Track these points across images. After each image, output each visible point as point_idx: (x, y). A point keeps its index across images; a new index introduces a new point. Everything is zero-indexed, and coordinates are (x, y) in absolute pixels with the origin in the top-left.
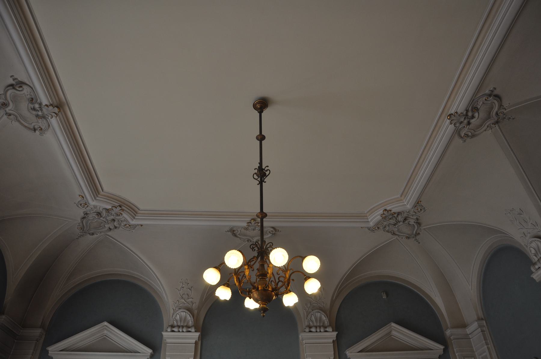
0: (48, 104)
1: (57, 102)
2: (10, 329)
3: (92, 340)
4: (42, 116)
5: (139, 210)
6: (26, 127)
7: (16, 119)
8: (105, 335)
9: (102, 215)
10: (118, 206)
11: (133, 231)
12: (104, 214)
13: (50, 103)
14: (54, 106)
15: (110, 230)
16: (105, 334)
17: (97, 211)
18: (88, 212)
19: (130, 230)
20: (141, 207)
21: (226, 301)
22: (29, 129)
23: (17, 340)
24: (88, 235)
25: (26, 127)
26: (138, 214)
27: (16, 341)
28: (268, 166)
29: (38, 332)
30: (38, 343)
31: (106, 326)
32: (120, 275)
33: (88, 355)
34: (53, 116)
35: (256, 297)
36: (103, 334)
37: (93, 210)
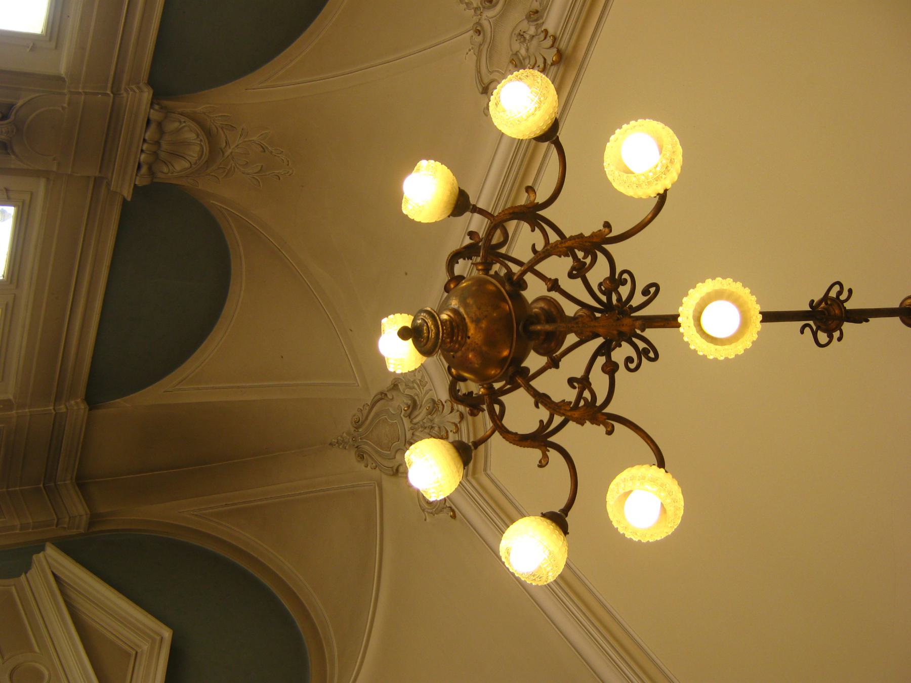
0: (551, 31)
1: (567, 47)
2: (61, 447)
3: (112, 631)
4: (521, 58)
5: (485, 470)
6: (479, 72)
7: (481, 45)
8: (137, 653)
9: (416, 413)
10: (458, 411)
11: (428, 520)
12: (422, 415)
13: (556, 33)
14: (556, 45)
15: (395, 471)
16: (139, 651)
17: (416, 398)
18: (400, 387)
19: (423, 511)
20: (494, 470)
21: (382, 360)
22: (481, 81)
23: (44, 486)
24: (353, 452)
25: (479, 72)
26: (474, 478)
27: (41, 485)
28: (840, 339)
29: (78, 509)
30: (54, 527)
31: (162, 639)
32: (307, 617)
33: (69, 633)
34: (537, 65)
35: (443, 315)
36: (137, 646)
37: (414, 388)
